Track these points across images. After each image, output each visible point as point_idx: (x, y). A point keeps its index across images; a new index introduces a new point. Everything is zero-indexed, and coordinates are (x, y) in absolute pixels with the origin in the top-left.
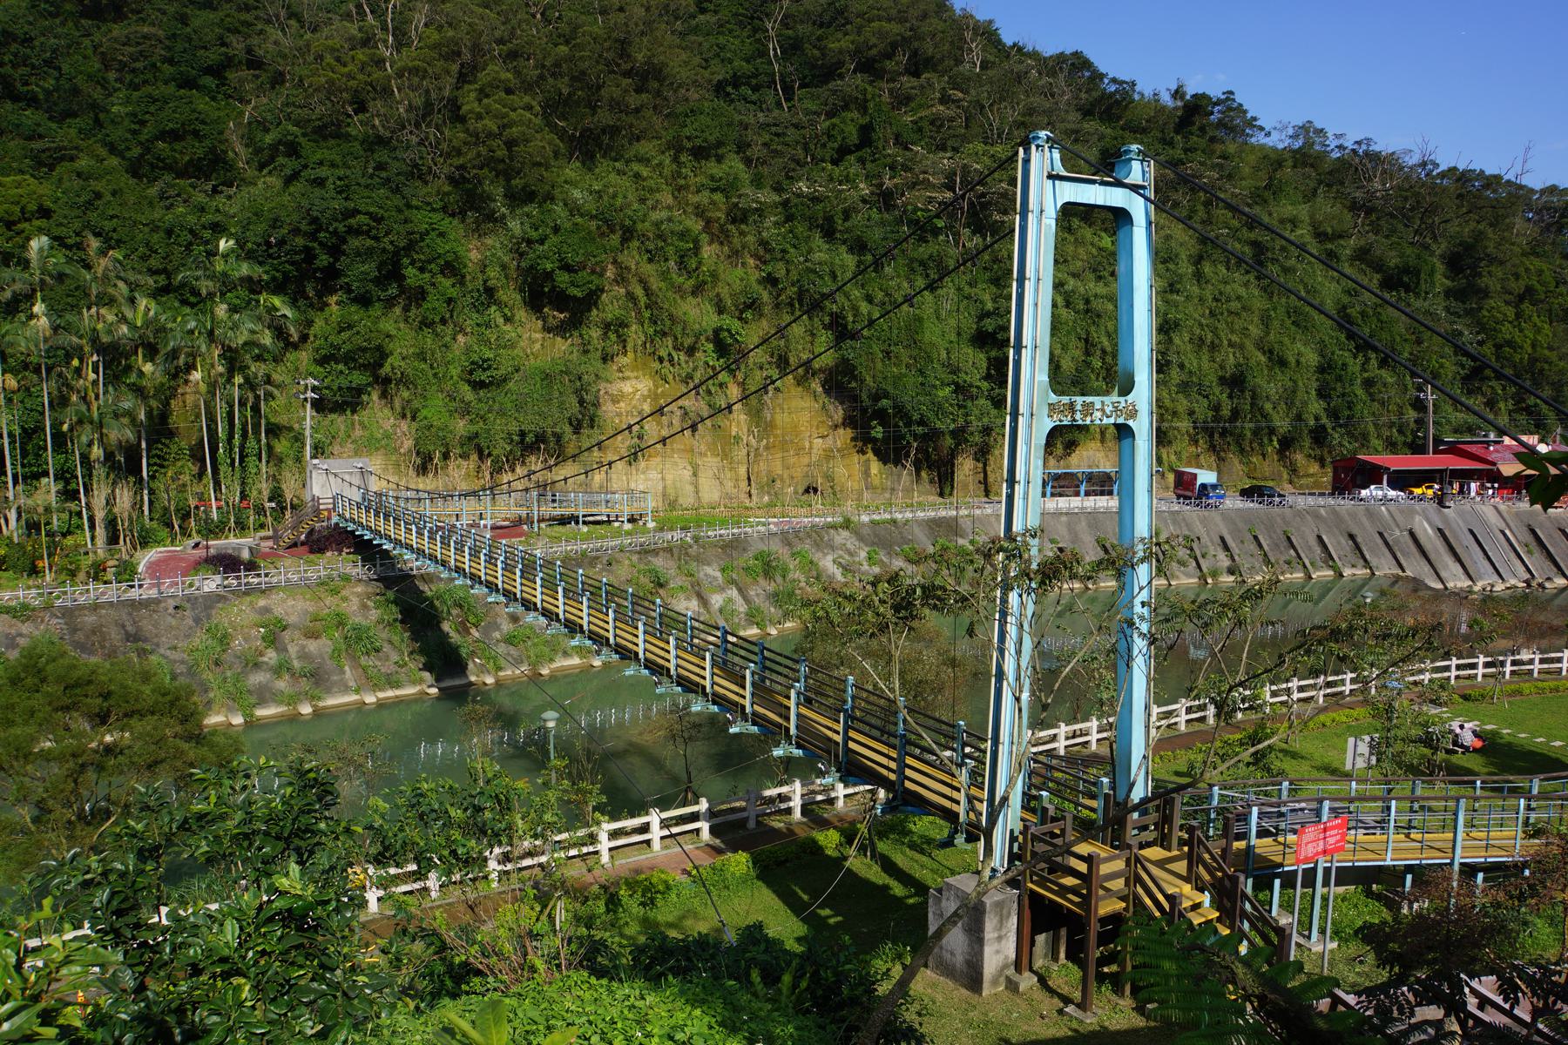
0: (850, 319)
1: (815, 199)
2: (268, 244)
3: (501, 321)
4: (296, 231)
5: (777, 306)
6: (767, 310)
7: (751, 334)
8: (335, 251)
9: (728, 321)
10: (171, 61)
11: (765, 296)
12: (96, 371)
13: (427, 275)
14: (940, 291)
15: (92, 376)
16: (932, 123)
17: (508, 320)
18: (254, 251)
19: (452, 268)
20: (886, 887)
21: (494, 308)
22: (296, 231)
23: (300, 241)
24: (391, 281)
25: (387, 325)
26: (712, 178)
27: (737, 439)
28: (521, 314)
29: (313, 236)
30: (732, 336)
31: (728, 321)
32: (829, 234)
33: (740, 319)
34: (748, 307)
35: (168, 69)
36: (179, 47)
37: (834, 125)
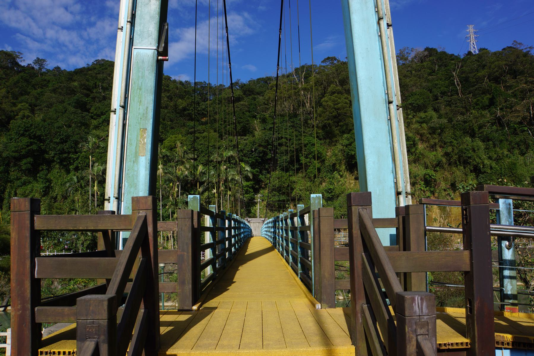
0: (482, 166)
1: (465, 122)
2: (252, 151)
3: (339, 177)
4: (260, 146)
5: (450, 164)
6: (446, 166)
7: (438, 176)
8: (275, 153)
9: (431, 172)
10: (249, 112)
11: (444, 160)
12: (178, 187)
13: (308, 159)
14: (526, 155)
15: (176, 189)
16: (522, 92)
17: (341, 176)
18: (246, 153)
19: (320, 158)
20: (300, 263)
21: (336, 172)
22: (260, 146)
23: (261, 148)
24: (295, 164)
25: (294, 178)
26: (421, 118)
27: (435, 220)
28: (347, 174)
29: (265, 147)
30: (430, 177)
31: (431, 172)
32: (473, 135)
33: (435, 171)
34: (437, 165)
35: (247, 113)
36: (252, 107)
37: (478, 100)
